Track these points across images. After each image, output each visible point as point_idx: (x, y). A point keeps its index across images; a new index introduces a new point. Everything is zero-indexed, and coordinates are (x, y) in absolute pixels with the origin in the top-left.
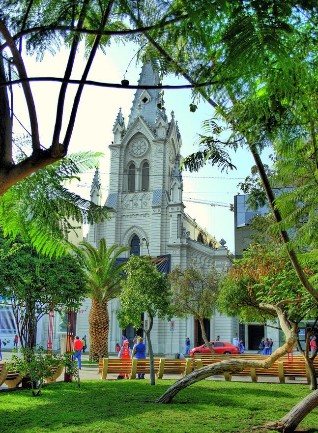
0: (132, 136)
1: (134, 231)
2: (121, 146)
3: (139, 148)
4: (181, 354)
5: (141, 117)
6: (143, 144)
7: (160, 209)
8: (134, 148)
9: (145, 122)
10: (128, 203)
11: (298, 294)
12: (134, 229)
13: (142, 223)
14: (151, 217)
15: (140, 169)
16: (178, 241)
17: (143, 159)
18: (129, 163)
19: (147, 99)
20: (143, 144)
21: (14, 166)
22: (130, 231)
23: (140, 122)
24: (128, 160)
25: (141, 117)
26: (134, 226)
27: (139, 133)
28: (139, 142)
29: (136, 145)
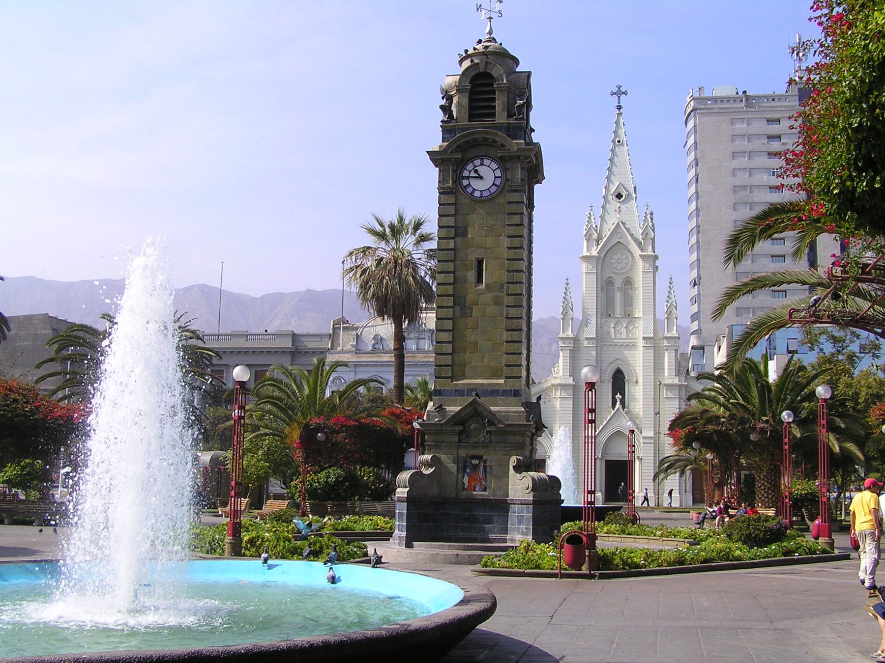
0: (608, 248)
2: (597, 259)
3: (619, 261)
4: (116, 611)
5: (622, 222)
6: (624, 256)
7: (652, 341)
8: (613, 261)
9: (628, 230)
11: (722, 425)
12: (618, 362)
15: (622, 288)
16: (676, 381)
17: (625, 276)
18: (607, 279)
19: (622, 196)
20: (624, 256)
21: (846, 426)
22: (611, 366)
23: (622, 229)
24: (606, 276)
25: (622, 222)
26: (618, 359)
27: (619, 242)
28: (619, 255)
29: (615, 257)
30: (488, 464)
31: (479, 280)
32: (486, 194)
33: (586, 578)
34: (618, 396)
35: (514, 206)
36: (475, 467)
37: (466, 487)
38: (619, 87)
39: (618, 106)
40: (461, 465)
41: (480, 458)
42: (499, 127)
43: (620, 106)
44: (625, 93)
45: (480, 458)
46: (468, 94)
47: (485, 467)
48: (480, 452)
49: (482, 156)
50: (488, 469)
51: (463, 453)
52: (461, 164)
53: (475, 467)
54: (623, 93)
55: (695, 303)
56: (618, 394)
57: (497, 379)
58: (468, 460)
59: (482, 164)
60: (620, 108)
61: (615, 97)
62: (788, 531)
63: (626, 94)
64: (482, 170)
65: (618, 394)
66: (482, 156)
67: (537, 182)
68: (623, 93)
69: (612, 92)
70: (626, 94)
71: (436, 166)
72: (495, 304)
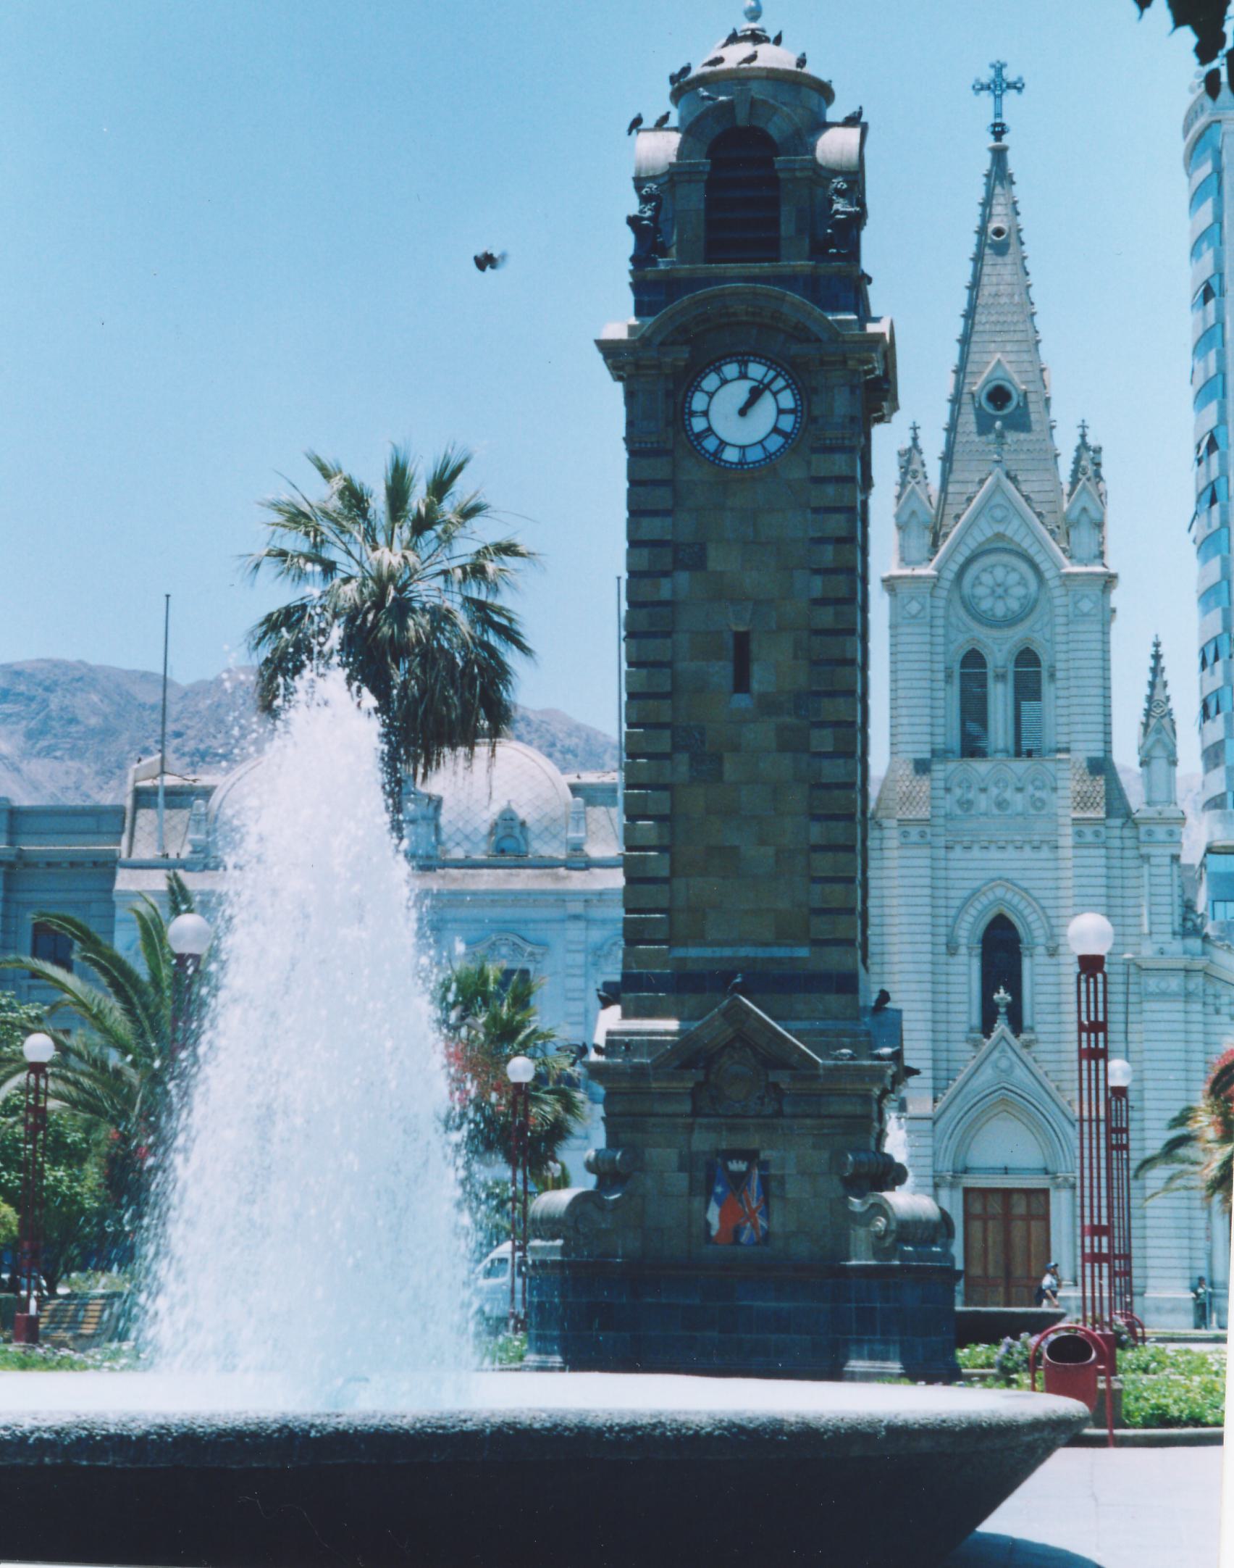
1: (1001, 900)
10: (971, 796)
13: (1028, 874)
14: (1062, 853)
30: (773, 1171)
31: (741, 683)
32: (755, 455)
33: (631, 1429)
34: (1002, 996)
35: (830, 490)
36: (738, 1181)
37: (714, 1233)
38: (999, 68)
39: (995, 125)
40: (701, 1175)
41: (750, 1156)
42: (788, 281)
43: (1002, 125)
44: (1017, 86)
45: (750, 1156)
46: (702, 185)
47: (764, 1181)
48: (753, 1141)
49: (743, 354)
50: (773, 1184)
51: (703, 1142)
52: (688, 379)
53: (738, 1181)
54: (1012, 86)
55: (1216, 658)
56: (1002, 991)
57: (791, 946)
58: (719, 1160)
59: (780, 412)
60: (1003, 132)
61: (987, 98)
62: (361, 833)
63: (1019, 90)
64: (765, 414)
65: (1002, 991)
66: (743, 354)
67: (880, 419)
68: (1012, 86)
69: (977, 81)
70: (1019, 90)
71: (618, 378)
72: (783, 747)
